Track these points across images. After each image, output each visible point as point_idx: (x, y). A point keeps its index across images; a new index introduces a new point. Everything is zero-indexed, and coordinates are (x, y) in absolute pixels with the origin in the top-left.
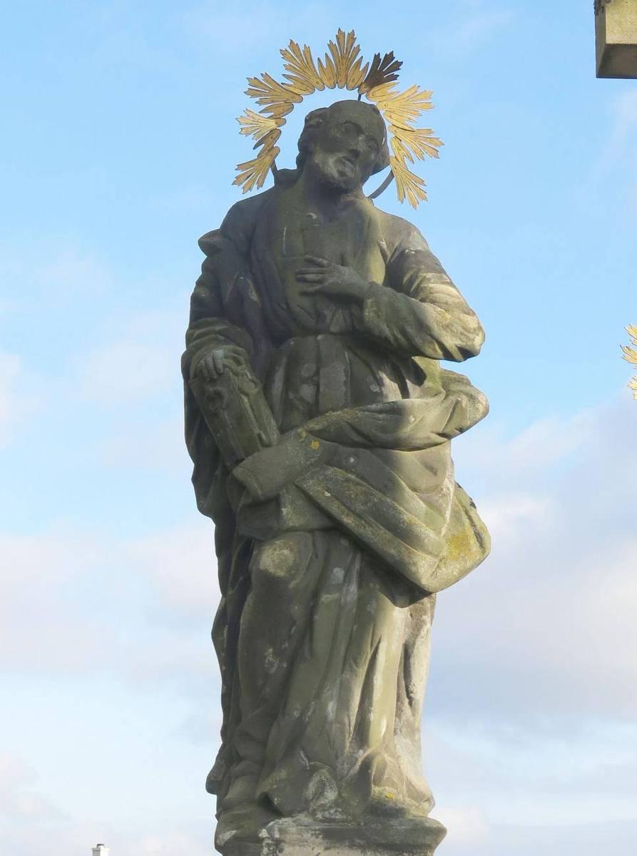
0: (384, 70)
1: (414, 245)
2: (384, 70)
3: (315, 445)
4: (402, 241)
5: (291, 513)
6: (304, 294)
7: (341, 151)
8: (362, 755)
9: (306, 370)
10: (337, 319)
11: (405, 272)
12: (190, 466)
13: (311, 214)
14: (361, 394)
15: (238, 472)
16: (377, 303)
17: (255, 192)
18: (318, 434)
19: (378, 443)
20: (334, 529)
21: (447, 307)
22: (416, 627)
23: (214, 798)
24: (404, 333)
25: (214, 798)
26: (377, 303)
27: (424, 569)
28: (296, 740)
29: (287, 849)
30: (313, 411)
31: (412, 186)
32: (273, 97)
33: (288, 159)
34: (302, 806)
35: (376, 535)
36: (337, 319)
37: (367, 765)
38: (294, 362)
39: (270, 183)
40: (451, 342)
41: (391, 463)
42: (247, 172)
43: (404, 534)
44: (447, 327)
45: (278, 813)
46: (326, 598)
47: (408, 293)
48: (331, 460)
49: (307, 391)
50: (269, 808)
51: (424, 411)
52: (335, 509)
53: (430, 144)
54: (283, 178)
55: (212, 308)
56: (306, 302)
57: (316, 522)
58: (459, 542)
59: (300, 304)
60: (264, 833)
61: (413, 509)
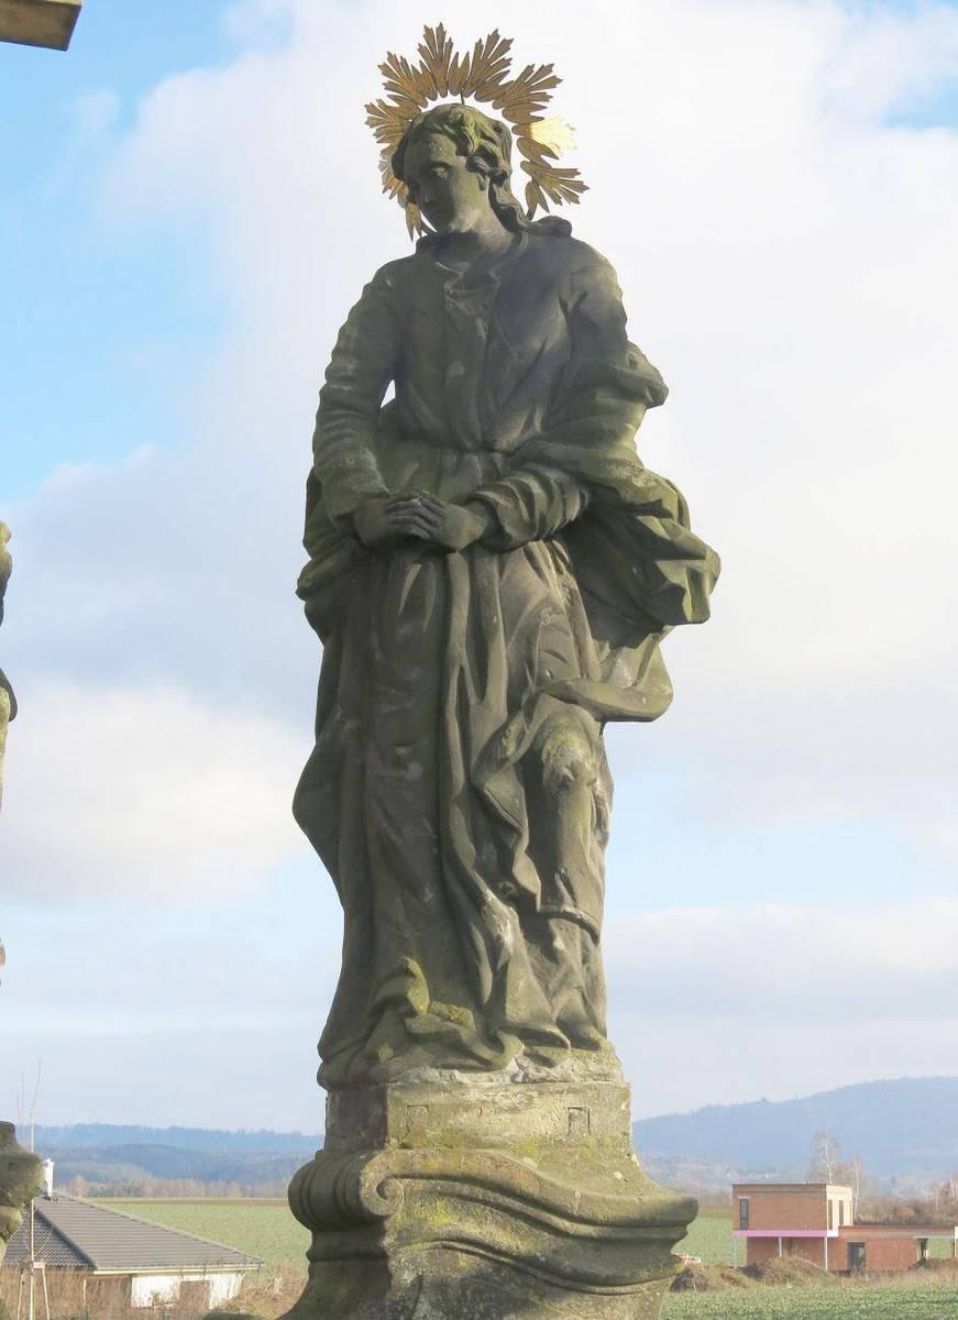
13: (414, 966)
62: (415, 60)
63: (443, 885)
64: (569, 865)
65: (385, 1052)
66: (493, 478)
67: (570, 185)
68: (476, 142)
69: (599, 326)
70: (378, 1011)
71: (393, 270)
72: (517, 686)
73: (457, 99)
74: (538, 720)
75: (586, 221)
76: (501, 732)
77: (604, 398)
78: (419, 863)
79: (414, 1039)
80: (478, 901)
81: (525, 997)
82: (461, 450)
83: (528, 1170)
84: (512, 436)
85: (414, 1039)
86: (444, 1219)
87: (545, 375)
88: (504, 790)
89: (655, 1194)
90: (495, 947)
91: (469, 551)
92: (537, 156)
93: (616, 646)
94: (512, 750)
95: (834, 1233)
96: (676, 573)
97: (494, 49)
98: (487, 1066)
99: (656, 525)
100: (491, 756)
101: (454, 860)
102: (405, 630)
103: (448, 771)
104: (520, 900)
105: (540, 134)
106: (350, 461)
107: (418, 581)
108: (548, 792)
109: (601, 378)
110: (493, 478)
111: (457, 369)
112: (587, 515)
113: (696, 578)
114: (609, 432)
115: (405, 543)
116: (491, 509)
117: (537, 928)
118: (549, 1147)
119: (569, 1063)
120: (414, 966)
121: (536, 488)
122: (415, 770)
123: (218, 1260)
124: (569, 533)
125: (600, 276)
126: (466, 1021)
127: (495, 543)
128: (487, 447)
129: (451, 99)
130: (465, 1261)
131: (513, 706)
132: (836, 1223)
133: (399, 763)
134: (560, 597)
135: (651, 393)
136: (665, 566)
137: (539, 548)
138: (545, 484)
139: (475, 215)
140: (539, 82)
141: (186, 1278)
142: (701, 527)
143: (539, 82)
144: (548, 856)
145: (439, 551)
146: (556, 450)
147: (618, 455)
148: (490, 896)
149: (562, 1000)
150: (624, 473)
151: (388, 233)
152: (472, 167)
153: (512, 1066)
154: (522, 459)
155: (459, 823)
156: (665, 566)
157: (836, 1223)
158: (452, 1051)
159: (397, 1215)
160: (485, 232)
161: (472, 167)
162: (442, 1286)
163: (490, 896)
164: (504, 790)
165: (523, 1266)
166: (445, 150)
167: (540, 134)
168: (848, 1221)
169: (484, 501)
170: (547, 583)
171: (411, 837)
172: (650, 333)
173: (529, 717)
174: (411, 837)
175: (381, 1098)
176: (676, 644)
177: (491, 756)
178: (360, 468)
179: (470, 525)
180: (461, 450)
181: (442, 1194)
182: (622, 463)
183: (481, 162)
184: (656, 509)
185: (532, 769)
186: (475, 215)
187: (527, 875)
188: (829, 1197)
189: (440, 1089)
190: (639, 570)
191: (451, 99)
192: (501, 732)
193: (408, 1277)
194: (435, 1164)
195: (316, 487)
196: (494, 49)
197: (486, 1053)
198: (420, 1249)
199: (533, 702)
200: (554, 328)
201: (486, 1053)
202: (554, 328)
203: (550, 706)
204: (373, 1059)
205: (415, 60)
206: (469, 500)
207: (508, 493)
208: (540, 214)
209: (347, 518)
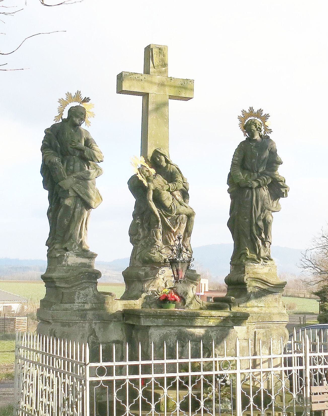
0: (87, 100)
1: (90, 138)
2: (87, 100)
3: (75, 179)
4: (313, 293)
5: (71, 193)
6: (71, 148)
7: (76, 116)
8: (81, 240)
9: (72, 163)
10: (78, 153)
11: (88, 142)
12: (42, 178)
13: (247, 248)
14: (82, 169)
15: (60, 184)
16: (87, 151)
17: (58, 122)
18: (75, 177)
19: (84, 179)
20: (78, 196)
21: (98, 152)
22: (88, 215)
23: (47, 248)
24: (91, 157)
25: (47, 248)
26: (87, 151)
27: (93, 204)
28: (71, 237)
29: (69, 257)
30: (73, 172)
31: (88, 123)
32: (63, 103)
33: (65, 116)
34: (72, 250)
35: (86, 198)
36: (78, 153)
37: (82, 242)
38: (68, 161)
39: (61, 121)
40: (99, 160)
41: (87, 183)
42: (57, 118)
43: (89, 197)
44: (99, 157)
45: (68, 251)
46: (77, 210)
47: (90, 148)
48: (78, 183)
49: (71, 168)
50: (66, 250)
51: (93, 172)
52: (79, 193)
53: (93, 115)
54: (64, 120)
55: (47, 146)
56: (72, 149)
57: (76, 195)
58: (97, 198)
59: (70, 149)
60: (65, 255)
61: (91, 192)
62: (248, 111)
63: (251, 236)
64: (269, 234)
65: (244, 261)
66: (259, 177)
67: (270, 131)
68: (258, 126)
69: (273, 153)
70: (241, 255)
71: (243, 143)
72: (262, 208)
73: (253, 118)
74: (265, 213)
75: (271, 136)
76: (260, 215)
77: (275, 165)
78: (248, 233)
79: (247, 259)
80: (256, 239)
81: (263, 254)
82: (254, 172)
83: (264, 277)
84: (261, 170)
85: (248, 259)
86: (254, 284)
87: (266, 161)
88: (260, 223)
89: (281, 281)
90: (259, 246)
91: (256, 188)
92: (266, 127)
93: (273, 201)
94: (262, 218)
95: (202, 294)
96: (283, 190)
97: (260, 111)
98: (259, 263)
99: (281, 183)
100: (259, 219)
101: (253, 233)
102: (246, 199)
103: (253, 221)
104: (262, 239)
105: (266, 124)
106: (238, 174)
107: (248, 193)
108: (267, 224)
109: (273, 161)
110: (259, 177)
111: (254, 160)
112: (271, 182)
113: (286, 191)
114: (275, 169)
115: (247, 187)
116: (259, 182)
117: (264, 243)
118: (266, 274)
119: (269, 262)
120: (247, 248)
121: (265, 179)
122: (247, 220)
123: (13, 300)
124: (269, 186)
125: (274, 145)
126: (255, 256)
127: (259, 186)
128: (257, 172)
129: (253, 118)
130: (257, 289)
131: (261, 211)
132: (203, 291)
133: (245, 219)
134: (267, 194)
135: (281, 163)
136: (282, 189)
137: (264, 187)
138: (266, 178)
139: (257, 137)
140: (267, 116)
141: (5, 305)
142: (287, 183)
143: (267, 116)
144: (266, 234)
145: (251, 188)
146: (268, 173)
147: (276, 173)
148: (258, 239)
149: (267, 253)
150: (277, 176)
151: (242, 137)
152: (257, 130)
153: (261, 263)
154: (263, 174)
155: (254, 228)
156: (282, 189)
157: (203, 291)
158: (253, 260)
159: (248, 283)
160: (258, 139)
161: (257, 130)
162: (254, 293)
163: (258, 239)
164: (260, 223)
165: (264, 290)
166: (254, 127)
167: (266, 124)
168: (207, 290)
169: (258, 181)
170: (265, 192)
171: (247, 230)
172: (280, 154)
173: (264, 213)
174: (247, 230)
175: (244, 267)
176: (281, 200)
177: (259, 219)
178: (240, 175)
179: (256, 184)
180: (254, 172)
181: (254, 280)
182: (277, 175)
183: (259, 129)
184: (282, 181)
185: (264, 220)
186: (257, 137)
187: (263, 236)
188: (201, 282)
189: (252, 266)
190: (277, 189)
191: (253, 118)
192: (260, 215)
193: (250, 291)
194: (253, 276)
195: (230, 175)
196: (260, 111)
197: (258, 261)
198: (251, 288)
199: (264, 211)
200: (267, 154)
201: (258, 261)
202: (267, 154)
203: (267, 211)
204: (242, 262)
205: (248, 111)
206: (255, 180)
207: (261, 179)
208: (265, 135)
209: (238, 183)
